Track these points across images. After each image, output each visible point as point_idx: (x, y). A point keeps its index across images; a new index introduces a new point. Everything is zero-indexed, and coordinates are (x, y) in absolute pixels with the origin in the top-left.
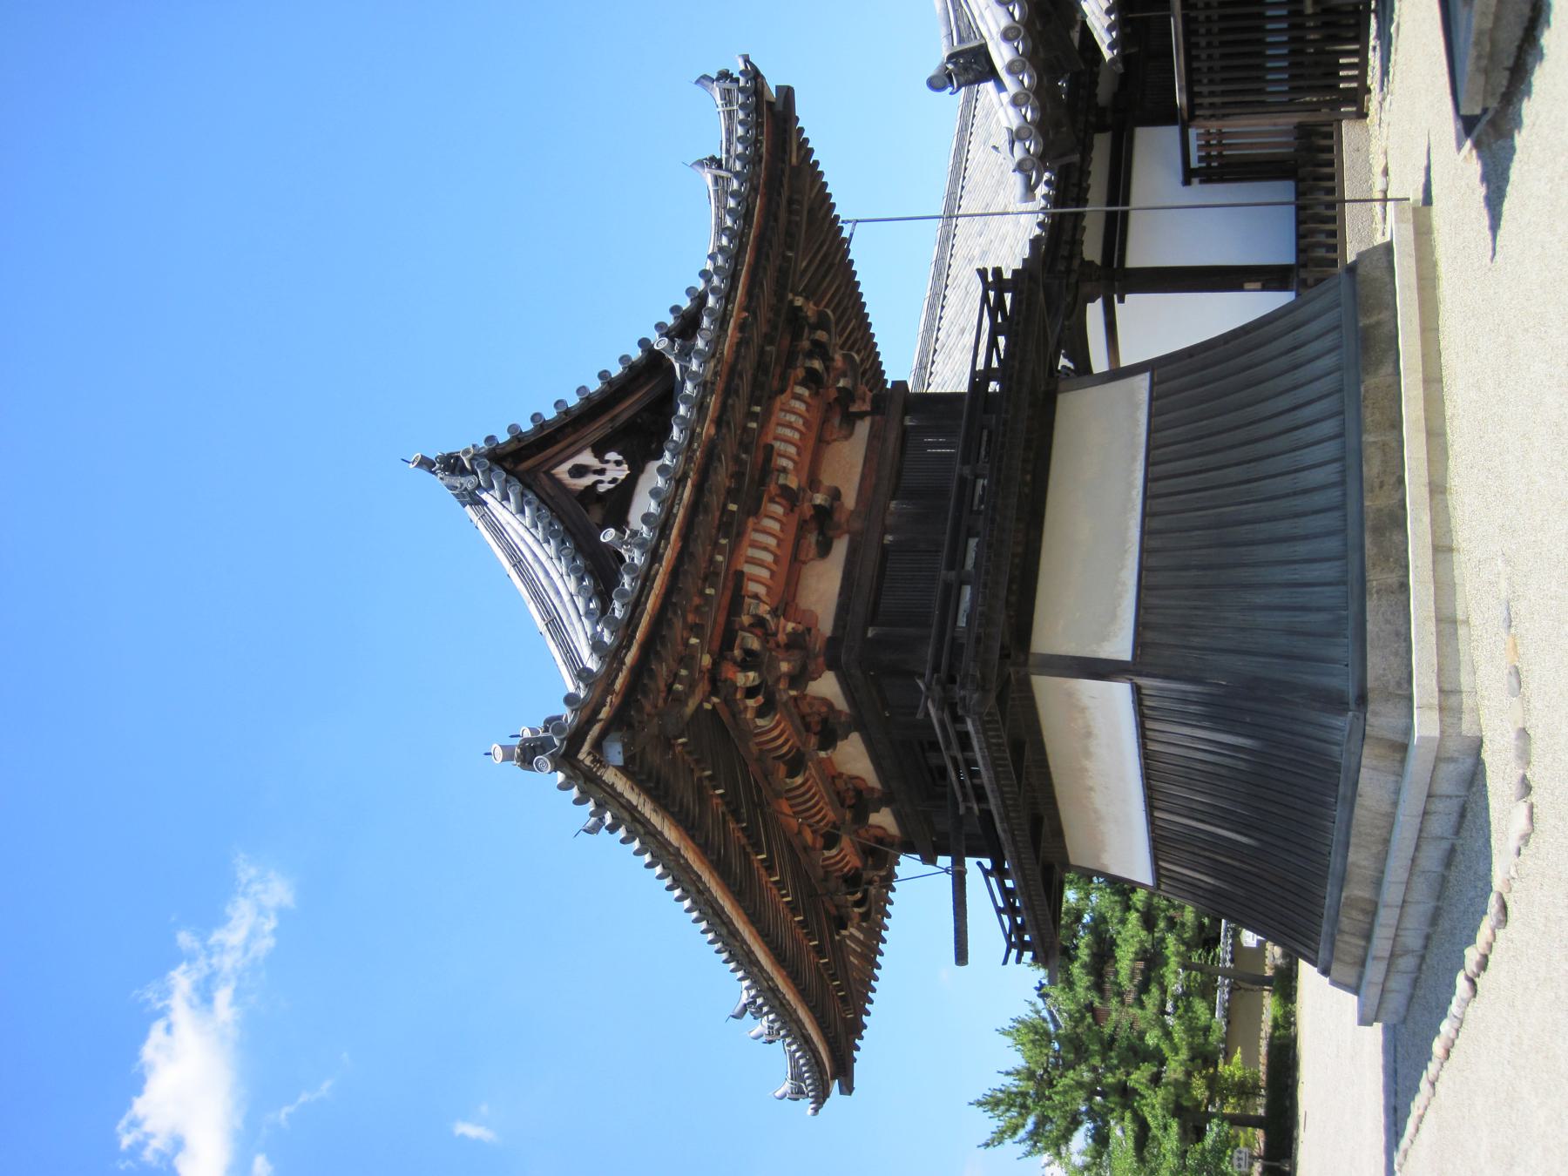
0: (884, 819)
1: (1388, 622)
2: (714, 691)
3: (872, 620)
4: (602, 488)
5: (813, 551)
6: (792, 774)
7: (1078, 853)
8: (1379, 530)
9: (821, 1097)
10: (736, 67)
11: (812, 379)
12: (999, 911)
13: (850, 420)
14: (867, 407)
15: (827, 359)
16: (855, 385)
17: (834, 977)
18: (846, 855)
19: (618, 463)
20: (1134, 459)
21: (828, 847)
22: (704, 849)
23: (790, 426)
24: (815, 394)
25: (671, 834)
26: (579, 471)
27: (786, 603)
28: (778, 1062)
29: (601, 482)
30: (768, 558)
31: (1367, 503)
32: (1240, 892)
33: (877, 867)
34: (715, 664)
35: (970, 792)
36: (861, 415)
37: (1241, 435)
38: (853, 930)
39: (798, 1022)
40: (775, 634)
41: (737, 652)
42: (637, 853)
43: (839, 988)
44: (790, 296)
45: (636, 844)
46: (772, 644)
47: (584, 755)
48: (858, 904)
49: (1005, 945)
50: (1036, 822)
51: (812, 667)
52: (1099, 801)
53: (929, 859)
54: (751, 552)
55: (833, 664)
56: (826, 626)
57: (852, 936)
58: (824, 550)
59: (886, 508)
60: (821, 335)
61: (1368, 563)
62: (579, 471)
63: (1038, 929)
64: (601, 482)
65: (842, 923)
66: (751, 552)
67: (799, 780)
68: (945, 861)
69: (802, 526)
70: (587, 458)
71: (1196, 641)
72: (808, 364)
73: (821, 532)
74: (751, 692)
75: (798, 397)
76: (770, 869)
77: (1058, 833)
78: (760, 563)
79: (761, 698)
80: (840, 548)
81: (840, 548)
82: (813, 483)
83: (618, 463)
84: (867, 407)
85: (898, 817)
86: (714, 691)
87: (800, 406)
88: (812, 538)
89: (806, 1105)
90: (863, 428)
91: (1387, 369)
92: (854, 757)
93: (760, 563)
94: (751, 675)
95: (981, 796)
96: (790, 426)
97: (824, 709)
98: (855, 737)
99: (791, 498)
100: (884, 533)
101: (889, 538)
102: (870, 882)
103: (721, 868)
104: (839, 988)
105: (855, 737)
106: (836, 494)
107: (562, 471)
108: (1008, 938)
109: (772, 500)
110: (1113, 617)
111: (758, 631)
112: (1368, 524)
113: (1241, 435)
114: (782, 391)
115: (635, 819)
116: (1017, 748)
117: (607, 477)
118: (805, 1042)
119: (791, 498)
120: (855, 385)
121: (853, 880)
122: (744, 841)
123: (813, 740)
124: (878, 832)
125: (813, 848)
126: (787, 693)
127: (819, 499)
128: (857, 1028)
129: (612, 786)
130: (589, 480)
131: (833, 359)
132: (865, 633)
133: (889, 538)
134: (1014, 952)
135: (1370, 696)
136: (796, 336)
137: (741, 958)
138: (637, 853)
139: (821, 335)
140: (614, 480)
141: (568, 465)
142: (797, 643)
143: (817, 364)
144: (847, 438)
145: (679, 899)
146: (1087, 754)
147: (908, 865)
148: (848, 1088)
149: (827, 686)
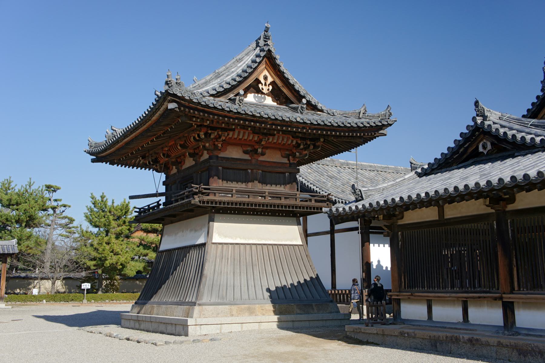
0: (174, 170)
1: (222, 311)
2: (198, 126)
3: (223, 168)
4: (260, 86)
5: (245, 149)
6: (181, 146)
7: (168, 228)
8: (249, 309)
9: (91, 154)
10: (392, 118)
11: (298, 145)
12: (149, 206)
13: (287, 157)
14: (291, 162)
15: (305, 149)
16: (297, 158)
17: (126, 157)
18: (163, 160)
19: (268, 90)
20: (274, 240)
21: (164, 155)
22: (152, 126)
23: (283, 140)
24: (294, 146)
25: (154, 118)
26: (266, 78)
27: (227, 143)
28: (101, 138)
29: (262, 85)
30: (241, 137)
31: (257, 305)
32: (157, 276)
33: (161, 168)
34: (205, 126)
35: (177, 198)
36: (289, 160)
37: (281, 270)
38: (142, 161)
39: (110, 149)
40: (217, 141)
41: (210, 131)
42: (148, 110)
43: (123, 158)
44: (161, 207)
45: (152, 107)
46: (214, 140)
47: (170, 98)
48: (149, 163)
49: (140, 207)
50: (174, 216)
51: (209, 152)
52: (180, 234)
53: (164, 183)
54: (242, 132)
55: (210, 158)
56: (222, 155)
57: (140, 161)
58: (245, 152)
59: (259, 170)
60: (312, 147)
61: (238, 306)
62: (266, 78)
63: (146, 216)
64: (262, 85)
65: (144, 157)
66: (242, 132)
67: (179, 148)
68: (162, 189)
69: (252, 146)
70: (270, 80)
71: (218, 260)
72: (302, 144)
73: (251, 151)
74: (199, 136)
75: (292, 141)
76: (152, 141)
77: (172, 222)
78: (238, 135)
79: (198, 139)
80: (247, 157)
81: (247, 157)
82: (265, 148)
83: (268, 90)
84: (291, 162)
85: (175, 174)
86: (198, 126)
87: (289, 142)
88: (249, 149)
89: (88, 148)
90: (285, 161)
91: (298, 311)
92: (189, 162)
93: (238, 135)
94: (203, 136)
95: (177, 201)
96: (283, 140)
97: (200, 154)
98: (194, 163)
99: (259, 142)
100: (251, 170)
101: (250, 171)
102: (156, 166)
103: (147, 130)
104: (123, 158)
105: (194, 163)
106: (263, 154)
107: (266, 73)
108: (142, 208)
109: (258, 137)
110: (226, 237)
111: (218, 136)
112: (251, 306)
113: (281, 270)
114: (293, 137)
115: (156, 109)
116: (174, 216)
117: (264, 87)
118: (105, 150)
119: (259, 142)
120: (297, 158)
121: (156, 161)
122: (158, 135)
123: (192, 151)
124: (171, 168)
125: (163, 150)
126: (201, 145)
127: (260, 150)
128: (112, 163)
129: (163, 104)
130: (263, 81)
131: (305, 150)
132: (221, 166)
133: (250, 171)
134: (138, 210)
135: (201, 307)
136: (311, 140)
137: (126, 134)
138: (148, 110)
139: (312, 147)
140: (263, 89)
141: (268, 74)
142: (216, 147)
143: (302, 147)
144: (282, 156)
145: (145, 113)
146: (191, 230)
147: (162, 177)
148: (93, 161)
149: (206, 156)
